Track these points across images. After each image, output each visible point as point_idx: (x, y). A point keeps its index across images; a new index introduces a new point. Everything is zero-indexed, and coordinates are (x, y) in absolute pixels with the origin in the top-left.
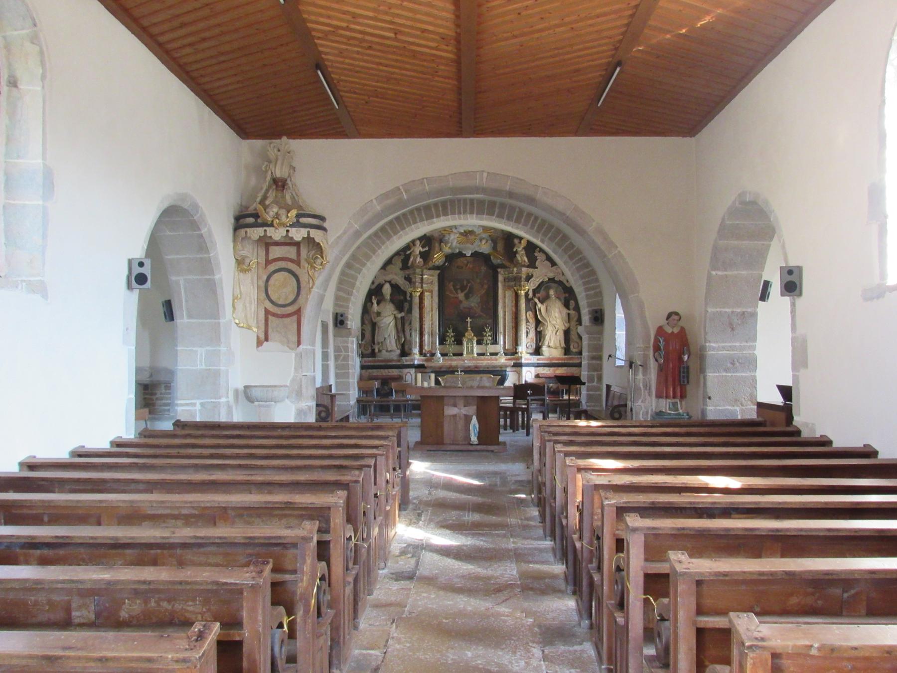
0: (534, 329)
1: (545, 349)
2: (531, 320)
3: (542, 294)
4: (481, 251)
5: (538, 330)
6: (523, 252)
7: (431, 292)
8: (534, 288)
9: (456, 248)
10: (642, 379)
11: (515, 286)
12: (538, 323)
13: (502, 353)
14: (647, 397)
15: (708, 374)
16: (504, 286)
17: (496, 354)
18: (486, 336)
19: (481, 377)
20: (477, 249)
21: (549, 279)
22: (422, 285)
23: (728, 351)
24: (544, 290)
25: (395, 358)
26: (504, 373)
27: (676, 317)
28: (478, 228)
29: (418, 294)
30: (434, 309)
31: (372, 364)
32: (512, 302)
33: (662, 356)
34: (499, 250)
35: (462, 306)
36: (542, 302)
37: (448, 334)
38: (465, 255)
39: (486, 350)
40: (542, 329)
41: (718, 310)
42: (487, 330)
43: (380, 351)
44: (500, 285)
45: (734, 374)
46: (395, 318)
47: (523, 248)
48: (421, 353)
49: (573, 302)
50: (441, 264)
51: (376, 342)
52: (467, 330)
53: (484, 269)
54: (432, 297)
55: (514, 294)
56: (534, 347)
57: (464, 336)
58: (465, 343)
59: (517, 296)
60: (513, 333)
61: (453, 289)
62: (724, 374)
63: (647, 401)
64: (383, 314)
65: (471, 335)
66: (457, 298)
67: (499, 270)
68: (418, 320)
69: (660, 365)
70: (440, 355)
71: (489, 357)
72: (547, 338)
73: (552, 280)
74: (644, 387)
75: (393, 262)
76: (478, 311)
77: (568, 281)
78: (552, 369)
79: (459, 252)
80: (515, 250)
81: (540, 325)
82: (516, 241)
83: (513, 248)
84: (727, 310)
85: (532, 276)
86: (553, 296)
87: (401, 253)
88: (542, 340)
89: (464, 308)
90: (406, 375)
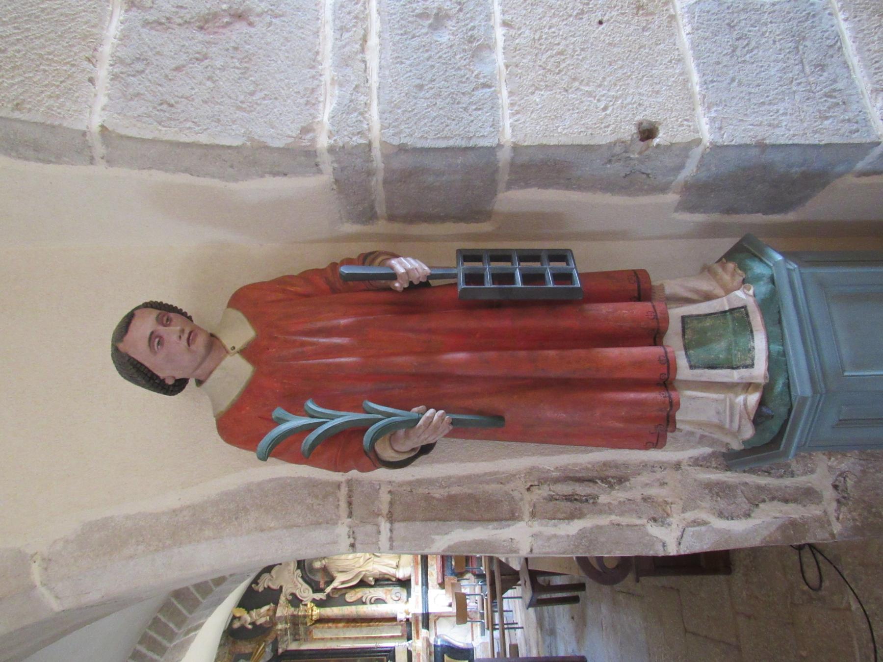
0: (371, 590)
1: (401, 574)
2: (359, 595)
3: (320, 579)
5: (373, 583)
6: (254, 613)
8: (311, 590)
10: (537, 527)
11: (306, 624)
12: (363, 584)
14: (635, 490)
15: (507, 137)
16: (306, 640)
17: (409, 653)
23: (365, 40)
26: (439, 649)
27: (145, 325)
32: (330, 628)
33: (401, 415)
34: (250, 650)
36: (332, 579)
40: (371, 579)
41: (103, 73)
44: (305, 647)
45: (498, 17)
47: (248, 613)
55: (318, 625)
56: (398, 589)
59: (322, 620)
60: (378, 625)
62: (499, 58)
63: (653, 492)
67: (280, 651)
69: (458, 430)
74: (581, 515)
80: (250, 627)
81: (365, 580)
82: (237, 625)
83: (247, 629)
84: (113, 29)
85: (293, 595)
88: (387, 576)
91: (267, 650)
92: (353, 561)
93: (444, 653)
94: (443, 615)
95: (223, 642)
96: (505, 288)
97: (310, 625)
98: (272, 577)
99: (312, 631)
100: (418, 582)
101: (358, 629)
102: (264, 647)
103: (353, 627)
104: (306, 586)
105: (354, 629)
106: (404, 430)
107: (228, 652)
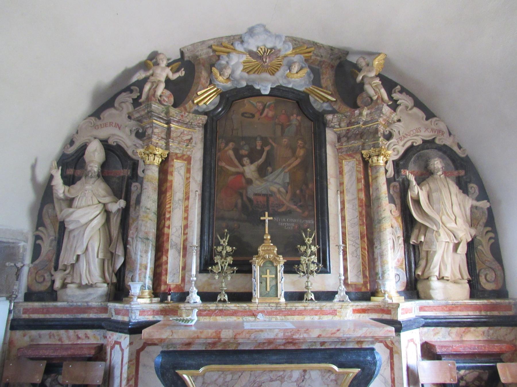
4: (290, 86)
7: (188, 160)
8: (396, 158)
9: (242, 78)
13: (343, 294)
16: (339, 150)
18: (305, 253)
19: (305, 371)
20: (282, 82)
21: (424, 142)
22: (167, 144)
24: (415, 162)
25: (94, 304)
28: (285, 42)
29: (158, 161)
30: (192, 195)
31: (41, 316)
35: (251, 191)
37: (219, 249)
38: (258, 94)
39: (307, 287)
40: (422, 239)
42: (309, 240)
43: (64, 286)
44: (330, 151)
46: (107, 213)
48: (156, 292)
49: (474, 186)
50: (212, 107)
51: (60, 266)
52: (262, 241)
53: (296, 119)
54: (188, 171)
57: (257, 253)
58: (256, 269)
61: (233, 157)
64: (76, 203)
65: (268, 251)
66: (242, 174)
68: (153, 217)
70: (198, 299)
71: (317, 305)
72: (437, 259)
73: (428, 144)
75: (116, 104)
76: (286, 199)
77: (460, 147)
78: (455, 330)
79: (247, 86)
80: (360, 78)
86: (440, 173)
87: (132, 88)
89: (256, 195)
90: (112, 348)
91: (325, 105)
92: (450, 212)
93: (363, 369)
94: (395, 356)
95: (336, 51)
96: (468, 363)
97: (362, 155)
98: (411, 109)
99: (354, 158)
100: (425, 311)
101: (356, 220)
102: (328, 100)
103: (361, 213)
104: (402, 151)
105: (357, 214)
106: (250, 261)
107: (324, 59)
